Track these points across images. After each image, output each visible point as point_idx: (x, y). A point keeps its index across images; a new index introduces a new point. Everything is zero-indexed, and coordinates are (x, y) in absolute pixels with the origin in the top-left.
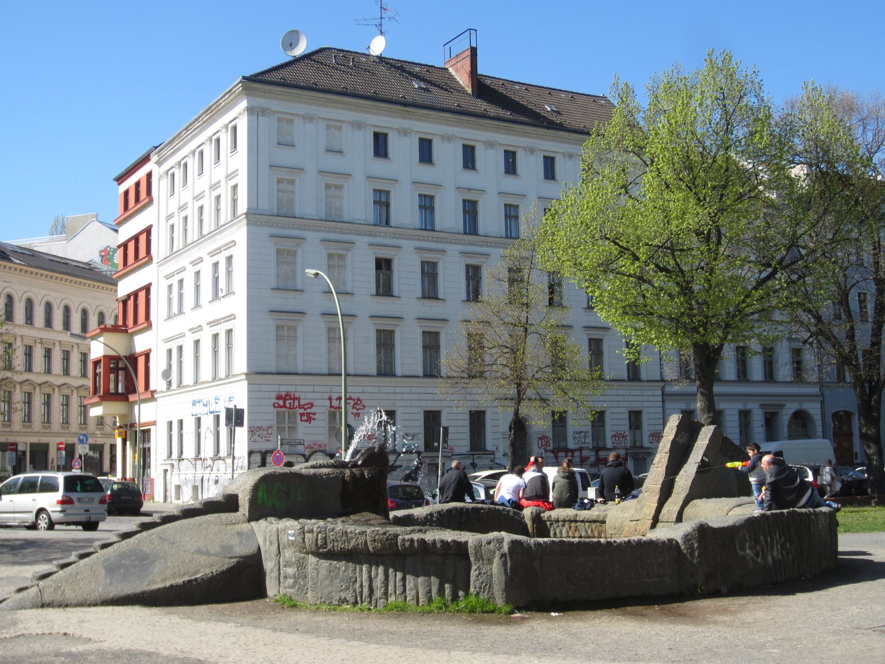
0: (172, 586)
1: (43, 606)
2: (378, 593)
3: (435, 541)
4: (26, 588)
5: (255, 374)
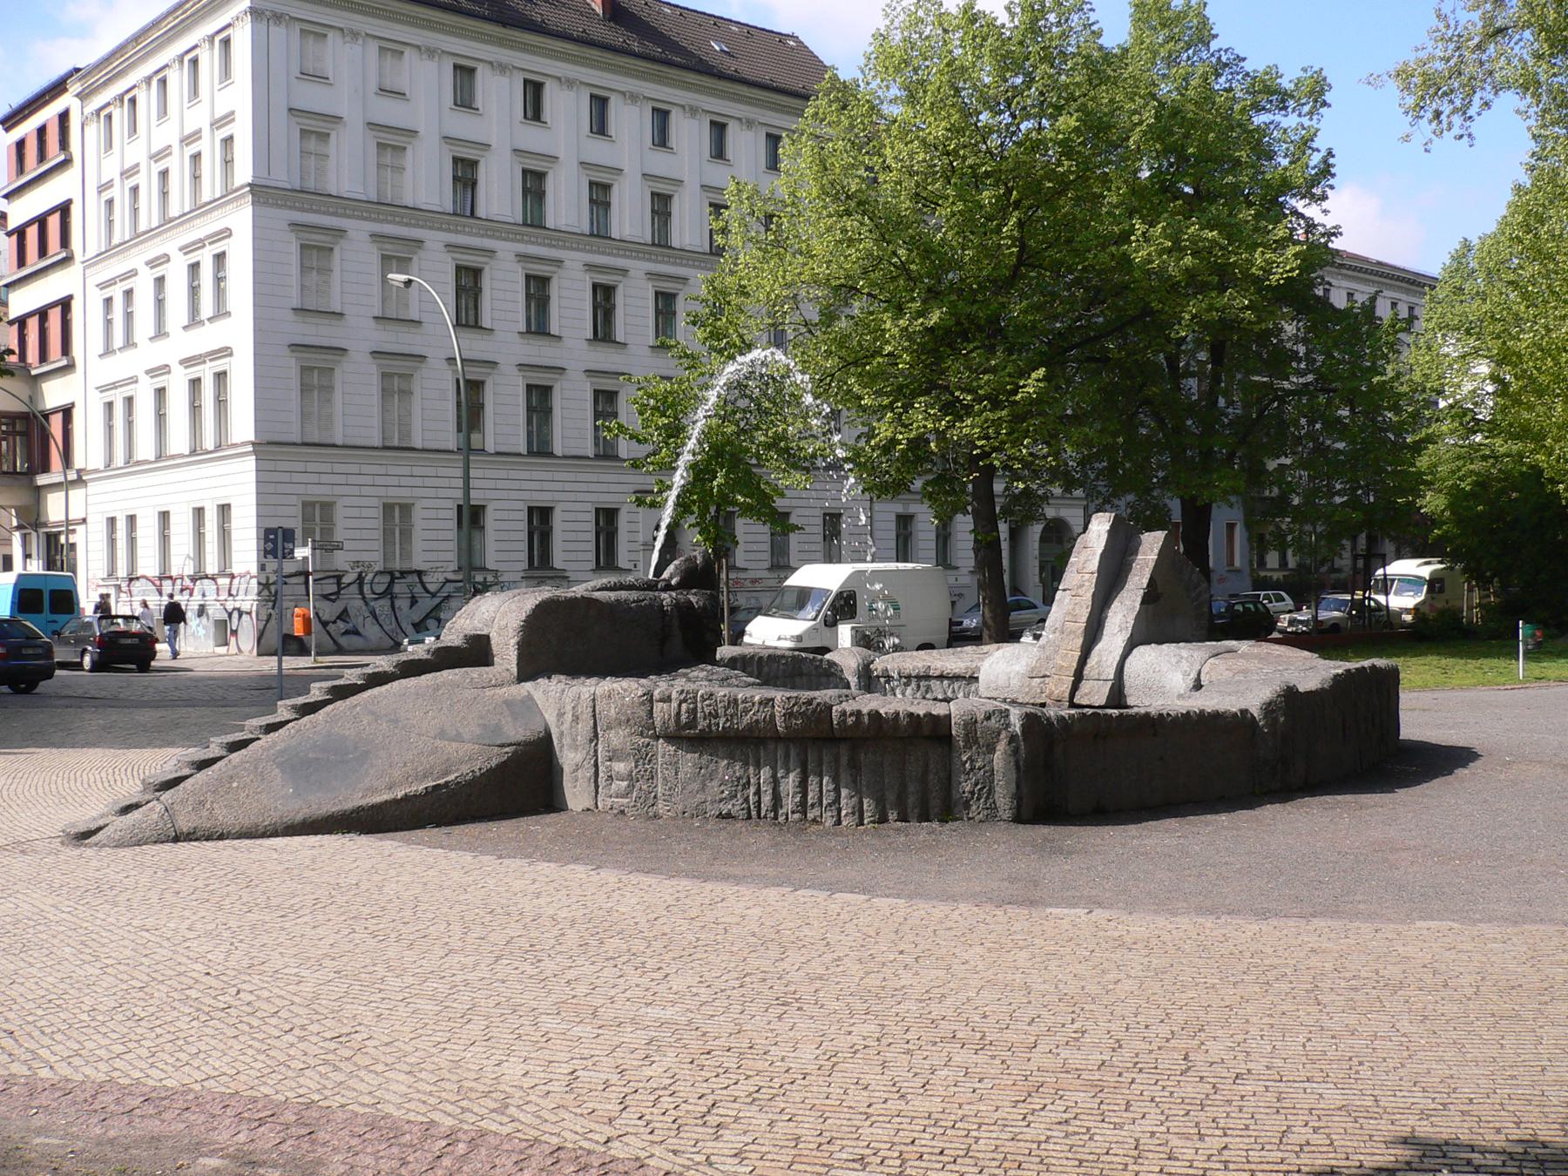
0: (406, 798)
1: (176, 839)
2: (789, 803)
3: (897, 714)
4: (136, 806)
5: (266, 448)
